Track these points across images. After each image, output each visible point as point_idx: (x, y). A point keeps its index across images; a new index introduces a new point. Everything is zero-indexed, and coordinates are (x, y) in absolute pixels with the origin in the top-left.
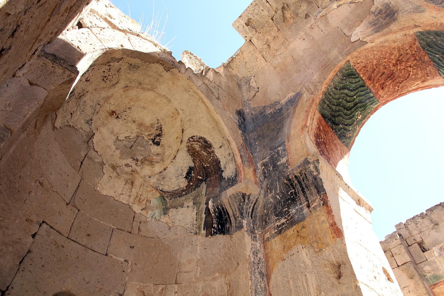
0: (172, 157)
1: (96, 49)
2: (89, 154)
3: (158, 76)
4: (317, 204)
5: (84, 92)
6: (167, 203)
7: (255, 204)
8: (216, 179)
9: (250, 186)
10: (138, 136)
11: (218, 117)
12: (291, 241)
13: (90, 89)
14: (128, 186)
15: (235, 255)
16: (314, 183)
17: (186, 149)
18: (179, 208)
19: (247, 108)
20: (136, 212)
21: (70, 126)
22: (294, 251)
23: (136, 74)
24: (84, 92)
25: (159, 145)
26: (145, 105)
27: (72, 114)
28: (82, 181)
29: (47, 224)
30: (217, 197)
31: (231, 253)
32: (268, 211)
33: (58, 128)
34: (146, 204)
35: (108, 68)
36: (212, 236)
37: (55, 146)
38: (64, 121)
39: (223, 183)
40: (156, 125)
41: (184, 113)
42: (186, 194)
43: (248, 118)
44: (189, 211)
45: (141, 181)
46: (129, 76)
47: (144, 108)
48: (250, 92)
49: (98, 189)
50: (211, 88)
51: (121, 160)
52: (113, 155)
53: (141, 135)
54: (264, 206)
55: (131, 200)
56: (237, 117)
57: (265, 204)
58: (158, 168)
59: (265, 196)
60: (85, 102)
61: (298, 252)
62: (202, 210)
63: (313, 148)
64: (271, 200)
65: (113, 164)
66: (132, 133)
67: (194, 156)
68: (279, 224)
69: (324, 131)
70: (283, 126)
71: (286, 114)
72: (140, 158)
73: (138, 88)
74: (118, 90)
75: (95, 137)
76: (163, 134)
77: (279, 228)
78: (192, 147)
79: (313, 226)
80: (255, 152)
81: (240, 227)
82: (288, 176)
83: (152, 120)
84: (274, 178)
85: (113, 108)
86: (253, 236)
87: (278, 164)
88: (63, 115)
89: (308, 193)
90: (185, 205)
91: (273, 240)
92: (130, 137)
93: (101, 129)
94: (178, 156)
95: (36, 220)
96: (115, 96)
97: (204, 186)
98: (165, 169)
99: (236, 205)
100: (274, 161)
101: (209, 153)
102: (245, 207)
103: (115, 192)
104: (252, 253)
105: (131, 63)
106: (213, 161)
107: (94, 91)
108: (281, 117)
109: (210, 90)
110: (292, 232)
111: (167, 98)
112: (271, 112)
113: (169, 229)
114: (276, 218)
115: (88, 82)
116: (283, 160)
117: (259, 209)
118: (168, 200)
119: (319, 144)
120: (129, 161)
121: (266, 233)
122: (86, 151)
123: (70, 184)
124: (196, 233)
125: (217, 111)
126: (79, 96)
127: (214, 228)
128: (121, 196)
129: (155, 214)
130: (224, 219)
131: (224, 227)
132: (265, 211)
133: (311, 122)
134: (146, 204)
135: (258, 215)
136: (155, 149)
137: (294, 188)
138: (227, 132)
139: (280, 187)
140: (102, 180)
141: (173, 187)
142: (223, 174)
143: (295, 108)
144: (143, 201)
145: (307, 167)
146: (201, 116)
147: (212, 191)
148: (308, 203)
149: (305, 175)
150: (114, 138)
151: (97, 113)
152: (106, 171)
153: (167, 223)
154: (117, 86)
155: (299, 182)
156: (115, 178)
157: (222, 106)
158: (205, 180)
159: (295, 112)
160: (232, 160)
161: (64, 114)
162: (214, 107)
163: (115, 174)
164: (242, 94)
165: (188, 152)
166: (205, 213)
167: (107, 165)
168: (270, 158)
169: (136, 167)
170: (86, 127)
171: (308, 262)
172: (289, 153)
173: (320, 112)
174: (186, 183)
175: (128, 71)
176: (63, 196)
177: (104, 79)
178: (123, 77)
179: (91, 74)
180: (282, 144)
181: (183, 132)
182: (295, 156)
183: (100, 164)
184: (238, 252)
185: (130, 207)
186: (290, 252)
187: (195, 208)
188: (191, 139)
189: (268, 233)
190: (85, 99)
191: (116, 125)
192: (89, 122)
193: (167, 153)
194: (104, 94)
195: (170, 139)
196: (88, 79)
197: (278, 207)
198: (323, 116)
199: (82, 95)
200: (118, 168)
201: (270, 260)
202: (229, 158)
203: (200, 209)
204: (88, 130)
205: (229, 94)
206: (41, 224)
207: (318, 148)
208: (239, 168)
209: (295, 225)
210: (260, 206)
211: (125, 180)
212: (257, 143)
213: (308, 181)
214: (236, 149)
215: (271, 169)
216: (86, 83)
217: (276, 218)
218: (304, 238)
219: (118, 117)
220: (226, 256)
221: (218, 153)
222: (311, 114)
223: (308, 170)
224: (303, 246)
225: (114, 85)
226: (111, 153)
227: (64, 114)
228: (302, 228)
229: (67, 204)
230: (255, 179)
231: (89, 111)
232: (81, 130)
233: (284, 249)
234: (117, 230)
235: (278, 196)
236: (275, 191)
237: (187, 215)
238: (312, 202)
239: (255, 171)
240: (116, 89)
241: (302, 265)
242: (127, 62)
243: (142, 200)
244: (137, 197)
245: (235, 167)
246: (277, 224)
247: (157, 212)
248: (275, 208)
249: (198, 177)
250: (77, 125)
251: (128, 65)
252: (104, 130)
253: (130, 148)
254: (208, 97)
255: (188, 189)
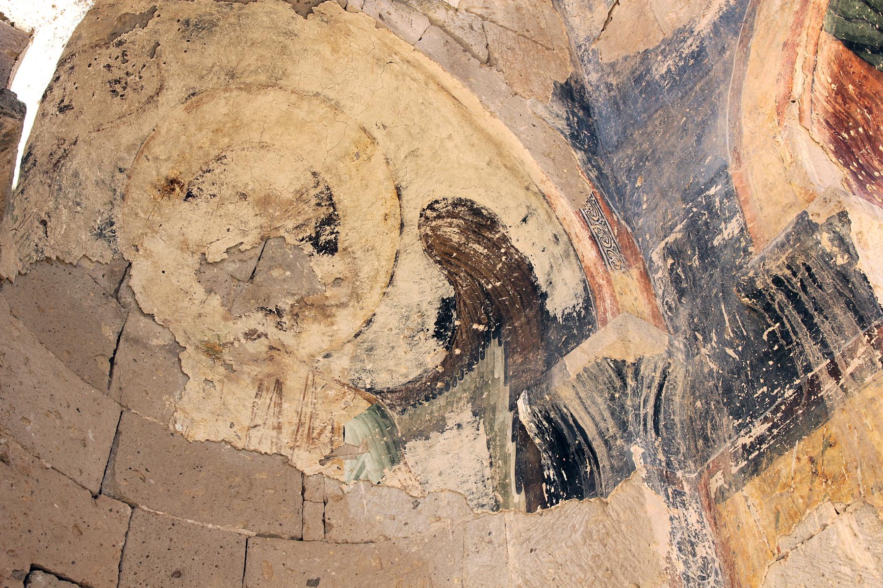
0: (383, 279)
1: (60, 7)
2: (129, 329)
3: (281, 39)
4: (861, 362)
5: (65, 146)
6: (394, 425)
7: (661, 386)
8: (529, 322)
9: (634, 335)
10: (265, 239)
11: (498, 127)
12: (796, 495)
13: (80, 130)
14: (267, 398)
15: (625, 559)
16: (841, 294)
17: (420, 246)
18: (433, 435)
19: (590, 67)
20: (307, 472)
21: (48, 259)
22: (810, 524)
23: (211, 49)
24: (65, 146)
25: (336, 250)
26: (266, 138)
27: (44, 223)
28: (125, 415)
29: (46, 571)
30: (538, 383)
31: (613, 555)
32: (708, 404)
33: (13, 277)
34: (332, 442)
35: (117, 52)
36: (544, 507)
37: (16, 334)
38: (26, 251)
39: (552, 335)
40: (313, 192)
41: (389, 134)
42: (447, 387)
43: (599, 100)
44: (466, 440)
45: (304, 375)
46: (192, 59)
47: (263, 146)
48: (590, 9)
49: (178, 427)
50: (458, 33)
51: (230, 323)
52: (203, 313)
53: (274, 234)
54: (693, 387)
55: (286, 438)
56: (560, 109)
57: (693, 382)
58: (346, 323)
59: (689, 355)
60: (76, 175)
61: (824, 527)
62: (502, 430)
63: (827, 172)
64: (712, 365)
65: (207, 342)
66: (244, 233)
67: (448, 262)
68: (747, 440)
69: (862, 95)
70: (714, 114)
71: (718, 67)
72: (286, 303)
73: (231, 90)
74: (169, 112)
75: (133, 272)
76: (340, 213)
77: (750, 453)
78: (438, 237)
79: (860, 440)
80: (638, 215)
81: (625, 469)
82: (752, 281)
83: (298, 179)
84: (710, 290)
85: (167, 171)
86: (670, 491)
87: (716, 243)
88: (19, 235)
89: (825, 327)
90: (450, 423)
91: (738, 497)
92: (242, 248)
93: (148, 243)
94: (400, 274)
95: (10, 569)
96: (163, 131)
97: (495, 351)
98: (369, 322)
99: (599, 400)
100: (699, 234)
101: (494, 245)
102: (629, 402)
103: (232, 425)
104: (675, 549)
105: (185, 17)
106: (510, 267)
107: (94, 134)
108: (703, 82)
109: (458, 40)
110: (794, 464)
111: (326, 100)
112: (669, 70)
113: (415, 507)
114: (736, 423)
115: (70, 113)
116: (729, 230)
117: (677, 399)
118: (394, 415)
119: (848, 148)
120: (256, 321)
121: (711, 475)
122: (118, 321)
123: (91, 436)
124: (497, 507)
125: (492, 108)
126: (50, 163)
127: (548, 481)
128: (253, 432)
129: (363, 467)
130: (572, 449)
131: (578, 474)
132: (698, 404)
133: (809, 79)
134: (332, 442)
135: (677, 419)
136: (325, 266)
137: (778, 319)
138: (534, 168)
139: (733, 320)
140: (185, 398)
141: (404, 371)
142: (549, 306)
143: (745, 43)
144: (320, 434)
145: (810, 243)
146: (445, 135)
147: (522, 364)
148: (832, 361)
149: (808, 269)
150: (194, 261)
151: (123, 198)
152: (193, 368)
153: (404, 488)
154: (162, 99)
155: (792, 296)
156: (221, 381)
157: (504, 87)
158: (497, 334)
159: (747, 55)
160: (568, 256)
161: (22, 231)
162: (480, 97)
163: (222, 370)
164: (566, 22)
165: (430, 254)
166: (514, 438)
167: (190, 349)
168: (686, 228)
169: (281, 335)
170: (99, 250)
171: (864, 559)
172: (746, 202)
173: (836, 35)
174: (442, 353)
175: (185, 45)
176: (76, 475)
177: (116, 87)
178: (174, 68)
179: (70, 86)
180: (718, 174)
181: (399, 196)
182: (769, 211)
183: (170, 351)
184: (633, 548)
185: (286, 461)
186: (800, 531)
187: (482, 427)
188: (429, 213)
189: (719, 474)
190: (72, 165)
191: (191, 220)
192: (105, 231)
193: (365, 271)
194: (128, 135)
195: (364, 223)
196: (66, 103)
197: (736, 384)
198: (853, 44)
199: (63, 157)
200: (226, 351)
201: (740, 562)
202: (558, 250)
203: (496, 429)
204: (108, 256)
205: (522, 36)
206: (27, 576)
207: (846, 165)
208: (593, 277)
209: (800, 439)
210: (680, 388)
211: (254, 380)
212: (638, 184)
213: (820, 287)
214: (575, 218)
215: (696, 263)
216: (61, 116)
217: (736, 423)
218: (836, 479)
219: (189, 195)
220: (599, 567)
221: (522, 239)
222: (803, 53)
223: (813, 253)
224: (839, 507)
225: (151, 99)
226: (195, 309)
227: (22, 231)
228: (825, 448)
229: (95, 497)
230: (650, 302)
231: (95, 198)
232: (86, 263)
233: (777, 520)
234: (259, 540)
235: (730, 352)
236: (720, 334)
237: (460, 454)
238: (843, 356)
239: (645, 276)
240: (162, 111)
241: (847, 570)
242: (172, 19)
243: (316, 432)
244: (300, 424)
245: (579, 275)
246: (741, 441)
247: (370, 461)
248: (728, 390)
249: (475, 326)
250: (69, 253)
251: (177, 26)
252: (157, 245)
253: (246, 280)
254: (453, 68)
255: (450, 372)
